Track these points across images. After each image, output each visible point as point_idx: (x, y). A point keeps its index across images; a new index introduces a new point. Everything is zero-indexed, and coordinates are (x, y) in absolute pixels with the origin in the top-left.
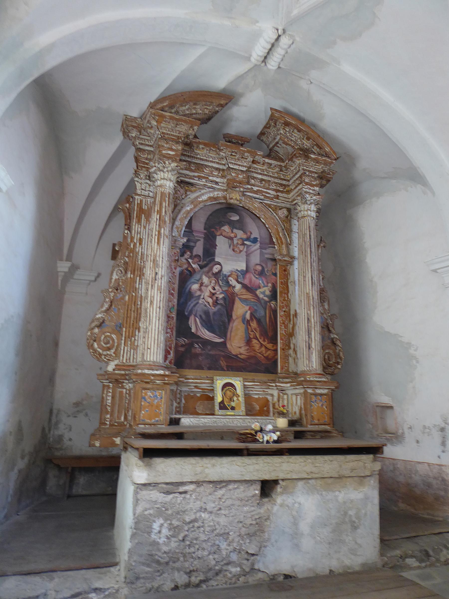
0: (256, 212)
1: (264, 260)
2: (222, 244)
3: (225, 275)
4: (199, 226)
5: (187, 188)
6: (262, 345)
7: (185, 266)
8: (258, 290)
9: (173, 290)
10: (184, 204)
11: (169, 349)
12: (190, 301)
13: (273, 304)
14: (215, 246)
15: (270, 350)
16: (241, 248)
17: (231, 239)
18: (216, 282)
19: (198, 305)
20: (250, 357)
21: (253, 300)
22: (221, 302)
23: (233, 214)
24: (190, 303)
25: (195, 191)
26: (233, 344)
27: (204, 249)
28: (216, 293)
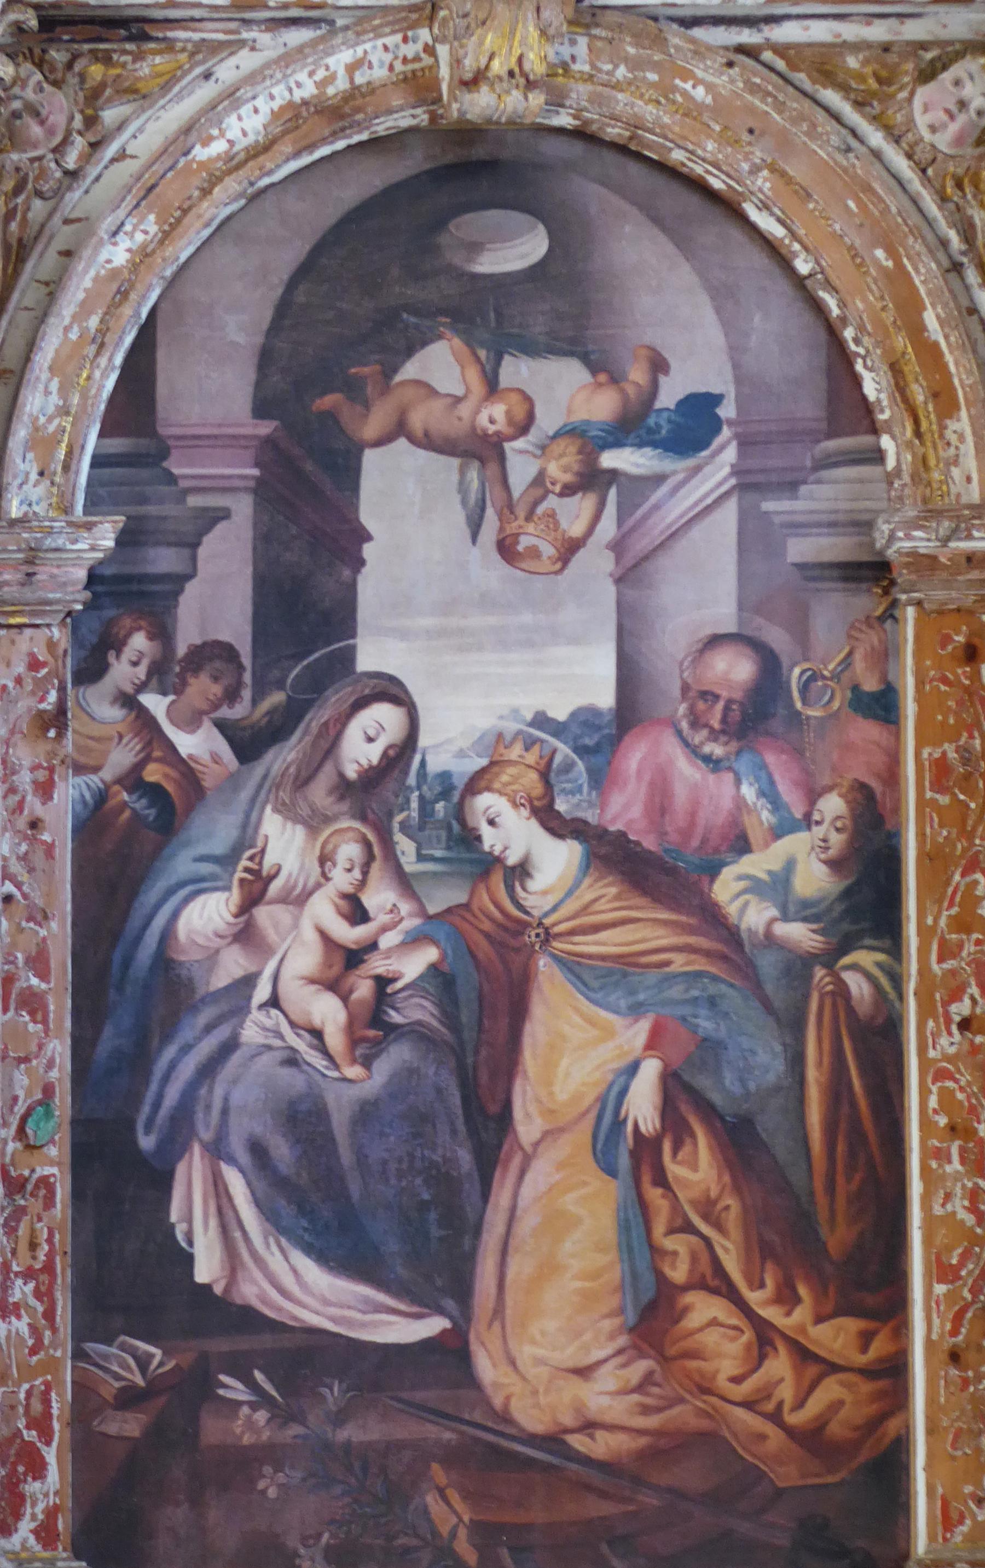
0: (705, 157)
1: (776, 592)
2: (405, 506)
3: (445, 776)
4: (212, 392)
5: (96, 71)
6: (764, 1338)
7: (121, 758)
8: (728, 873)
9: (39, 963)
10: (83, 224)
11: (30, 1435)
12: (167, 1038)
13: (859, 972)
14: (348, 543)
15: (833, 1368)
16: (574, 514)
17: (484, 451)
18: (370, 858)
19: (236, 1058)
20: (666, 1448)
21: (679, 963)
22: (416, 1011)
23: (494, 215)
24: (170, 1052)
25: (168, 82)
26: (526, 1353)
27: (261, 583)
28: (373, 946)
